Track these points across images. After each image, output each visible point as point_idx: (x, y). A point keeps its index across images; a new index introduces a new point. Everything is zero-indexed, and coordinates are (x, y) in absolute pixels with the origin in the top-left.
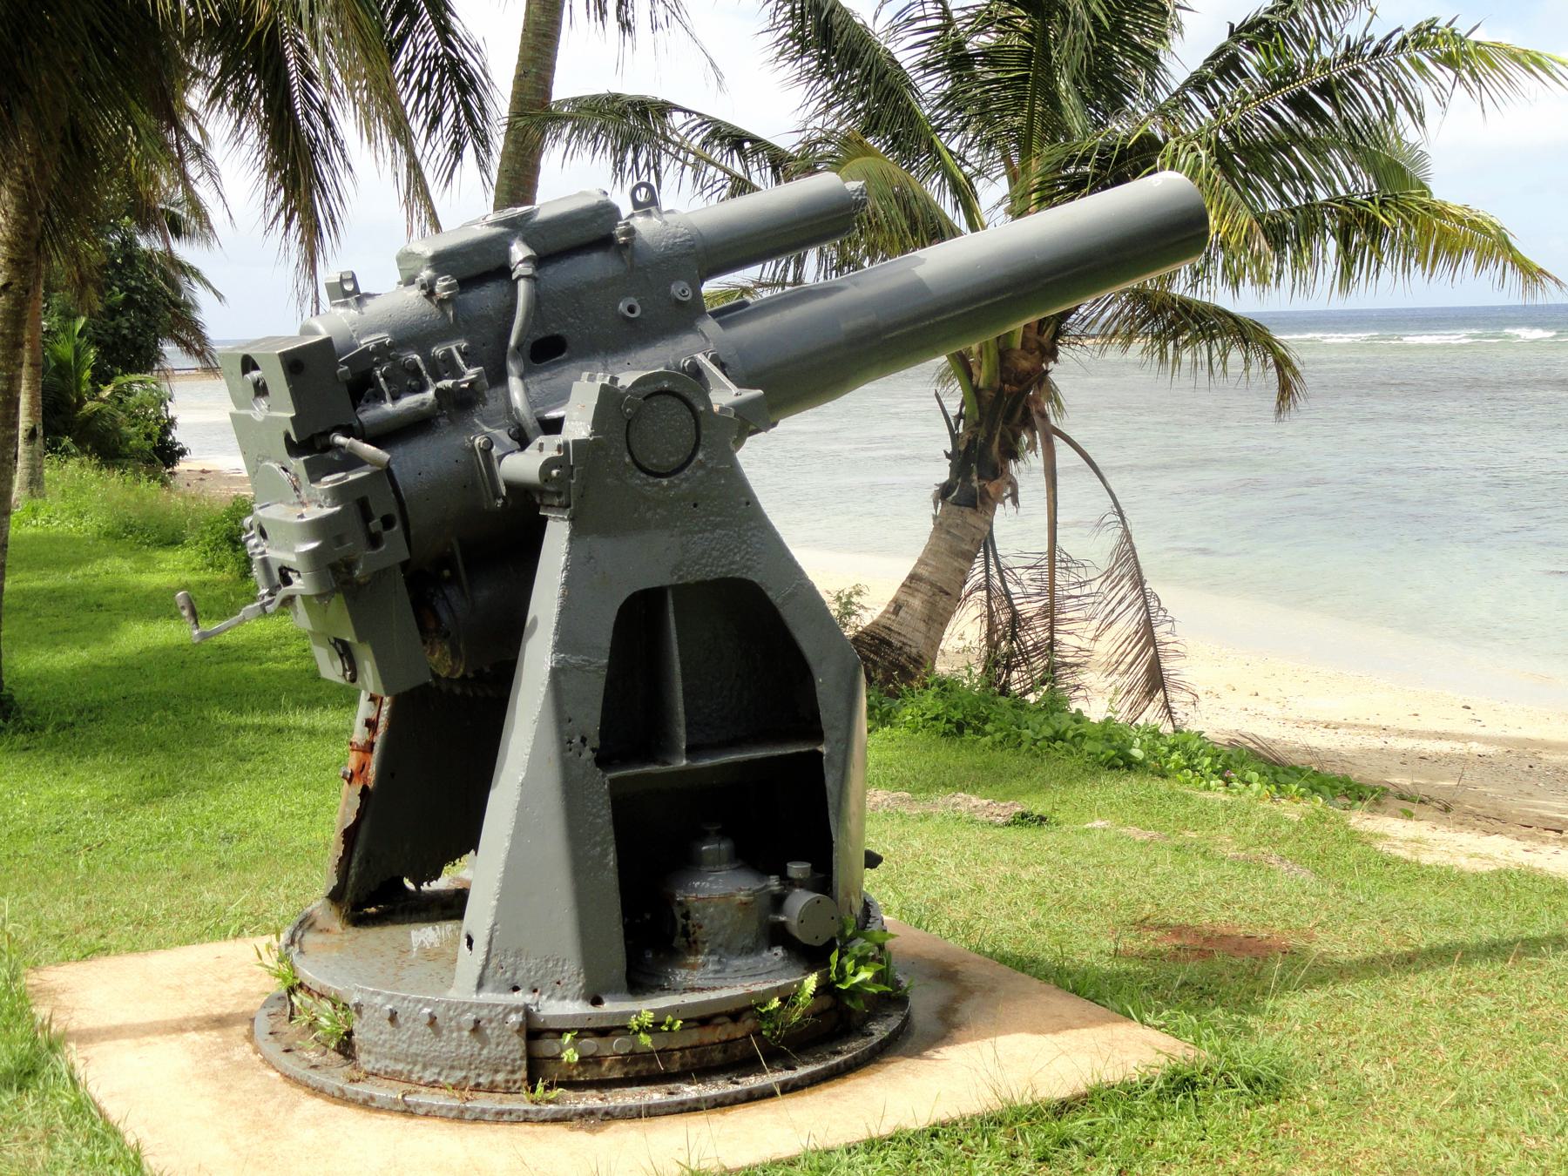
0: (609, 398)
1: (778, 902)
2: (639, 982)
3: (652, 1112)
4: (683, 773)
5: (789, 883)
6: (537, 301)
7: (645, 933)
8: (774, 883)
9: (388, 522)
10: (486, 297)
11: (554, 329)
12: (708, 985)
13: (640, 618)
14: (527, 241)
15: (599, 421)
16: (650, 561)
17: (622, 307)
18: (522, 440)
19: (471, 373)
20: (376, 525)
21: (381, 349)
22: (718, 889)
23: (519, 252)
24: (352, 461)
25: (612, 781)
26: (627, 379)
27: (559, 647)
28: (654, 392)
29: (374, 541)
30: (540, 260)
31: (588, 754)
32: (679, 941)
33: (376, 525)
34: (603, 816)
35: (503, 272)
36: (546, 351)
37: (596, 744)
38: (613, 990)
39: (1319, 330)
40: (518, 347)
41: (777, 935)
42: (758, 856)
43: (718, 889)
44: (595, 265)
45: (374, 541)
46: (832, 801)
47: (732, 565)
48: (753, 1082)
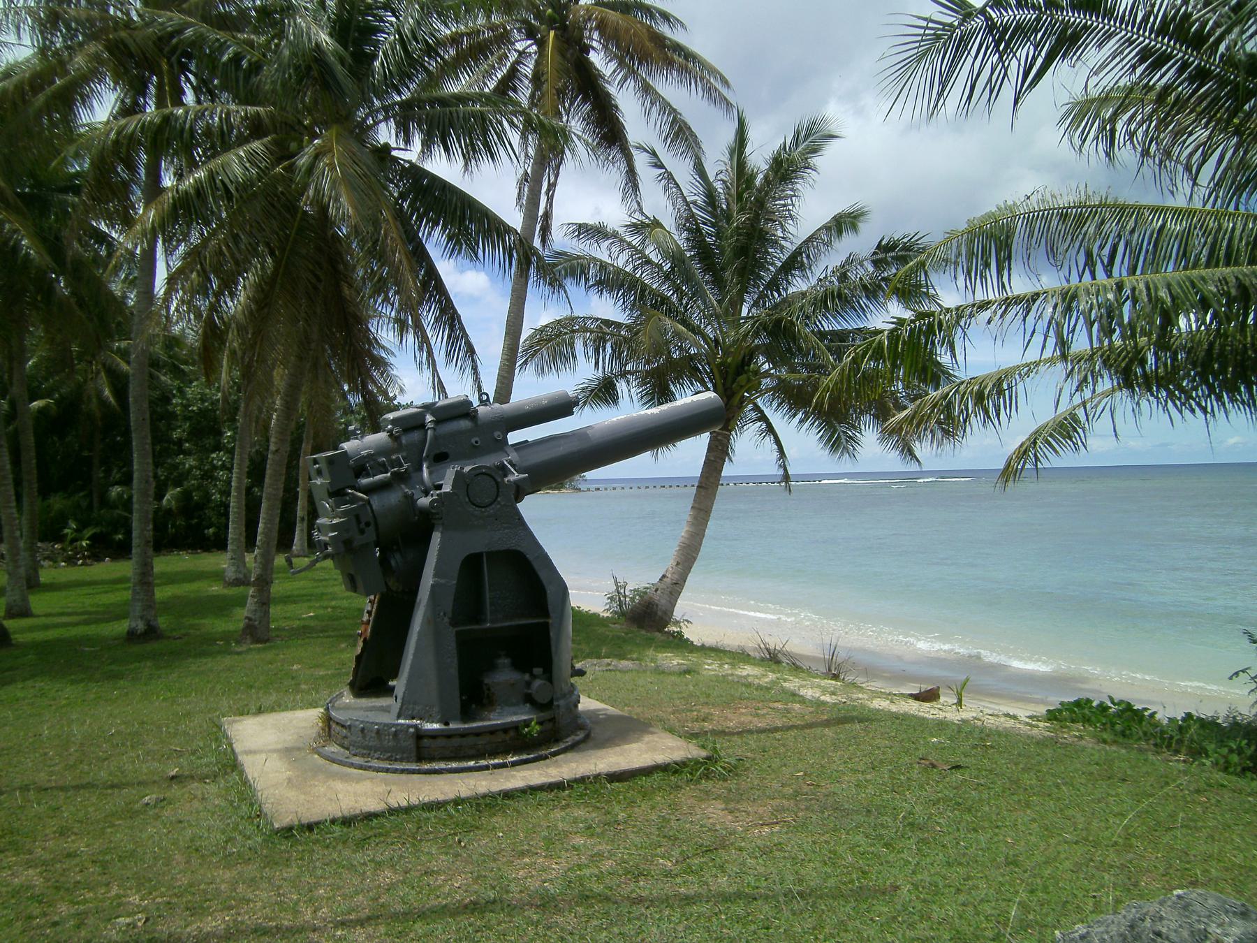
0: (459, 475)
1: (528, 684)
2: (466, 715)
3: (413, 772)
4: (490, 629)
5: (534, 677)
6: (435, 438)
7: (473, 697)
8: (527, 677)
9: (368, 524)
10: (416, 436)
11: (443, 450)
12: (497, 719)
13: (472, 564)
14: (432, 414)
15: (453, 486)
16: (482, 540)
17: (473, 441)
18: (426, 493)
19: (406, 466)
20: (362, 525)
21: (369, 455)
22: (504, 676)
23: (429, 418)
24: (354, 499)
25: (457, 633)
26: (467, 469)
27: (435, 576)
28: (477, 473)
29: (362, 532)
30: (437, 422)
31: (446, 620)
32: (485, 701)
33: (362, 525)
34: (451, 645)
35: (422, 426)
36: (440, 458)
37: (450, 615)
38: (454, 719)
39: (127, 398)
40: (427, 456)
41: (529, 699)
42: (522, 665)
43: (504, 676)
44: (465, 424)
45: (362, 532)
46: (553, 643)
47: (511, 544)
48: (483, 762)
